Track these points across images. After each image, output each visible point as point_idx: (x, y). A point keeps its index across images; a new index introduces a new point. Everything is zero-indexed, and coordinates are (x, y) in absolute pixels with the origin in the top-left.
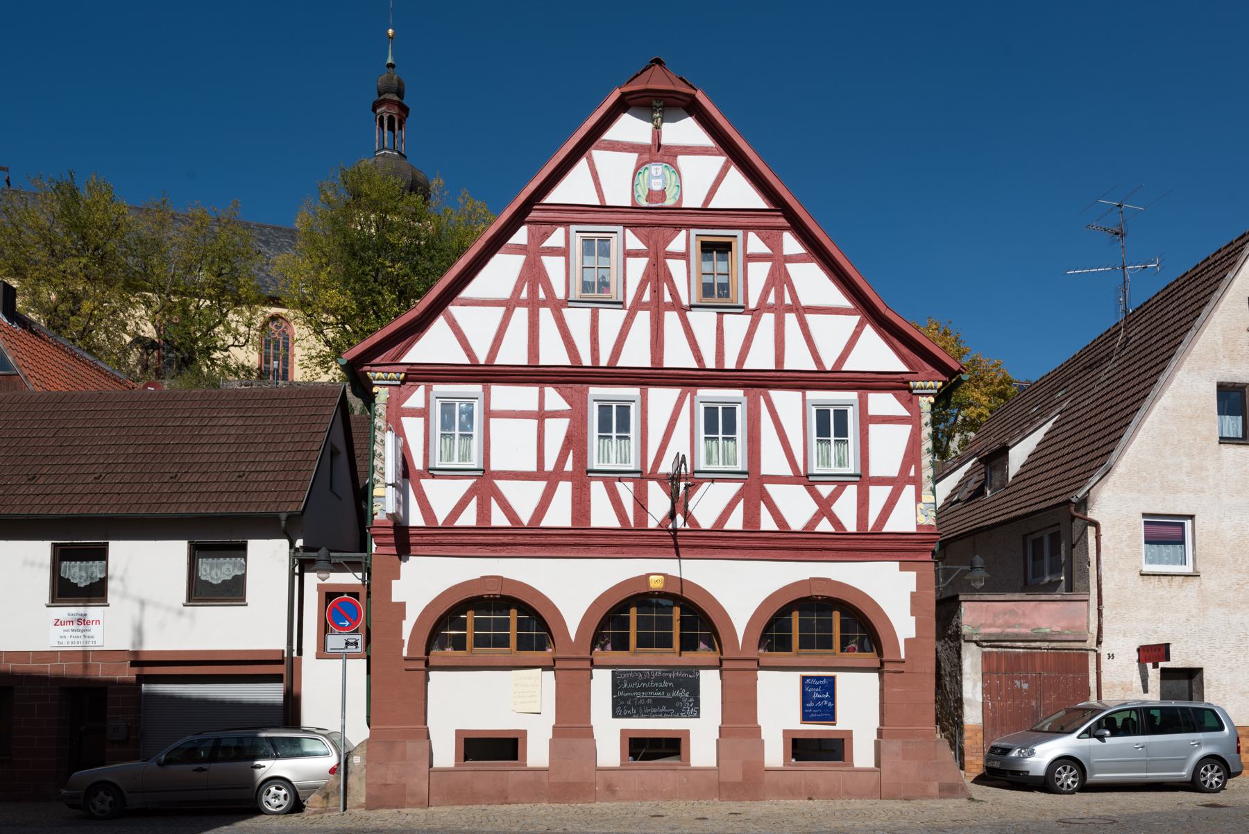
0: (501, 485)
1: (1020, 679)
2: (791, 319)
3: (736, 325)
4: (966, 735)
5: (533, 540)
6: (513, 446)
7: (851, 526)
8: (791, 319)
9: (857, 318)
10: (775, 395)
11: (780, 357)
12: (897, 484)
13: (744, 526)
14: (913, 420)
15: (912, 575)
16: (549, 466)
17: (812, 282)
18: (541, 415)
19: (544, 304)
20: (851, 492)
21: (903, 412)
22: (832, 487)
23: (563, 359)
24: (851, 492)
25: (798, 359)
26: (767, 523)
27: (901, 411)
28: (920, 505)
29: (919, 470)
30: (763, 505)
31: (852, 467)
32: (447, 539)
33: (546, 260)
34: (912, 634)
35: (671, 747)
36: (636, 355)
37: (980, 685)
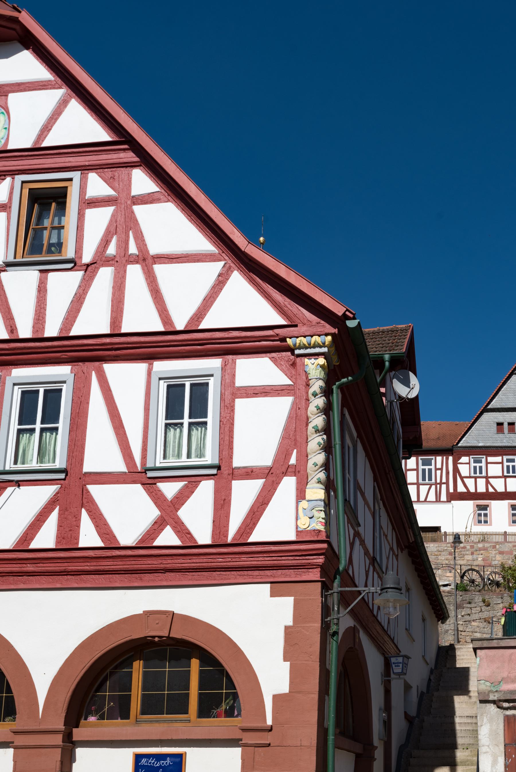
2: (134, 273)
3: (63, 285)
7: (203, 535)
8: (134, 273)
9: (218, 266)
10: (111, 369)
12: (270, 477)
13: (58, 542)
14: (298, 389)
15: (287, 604)
17: (166, 226)
20: (206, 489)
21: (284, 380)
22: (178, 485)
24: (206, 489)
25: (141, 318)
27: (279, 378)
28: (303, 504)
29: (304, 457)
30: (84, 515)
31: (210, 457)
34: (284, 688)
37: (501, 761)
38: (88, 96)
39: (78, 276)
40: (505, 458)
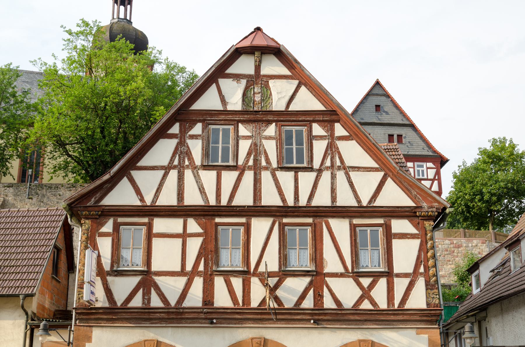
0: (157, 279)
2: (340, 175)
3: (306, 179)
6: (166, 256)
7: (383, 305)
8: (340, 175)
16: (189, 267)
18: (184, 236)
20: (383, 282)
21: (414, 231)
23: (277, 202)
24: (383, 282)
25: (346, 199)
26: (328, 303)
33: (190, 142)
39: (314, 175)
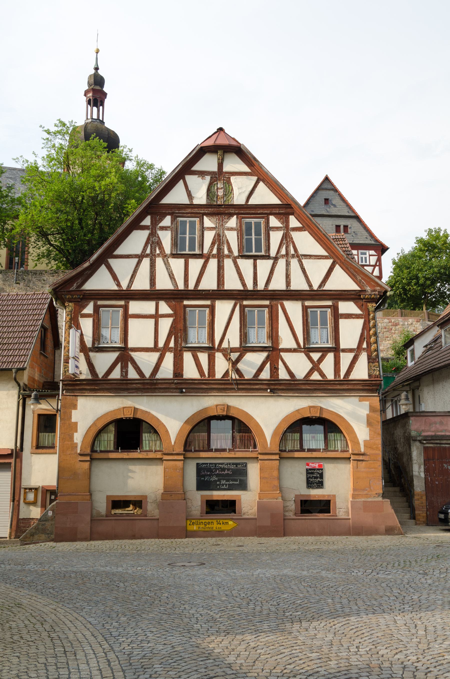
1: (446, 463)
2: (294, 262)
3: (264, 266)
4: (416, 497)
5: (150, 386)
6: (141, 334)
7: (330, 376)
8: (294, 262)
10: (288, 304)
11: (288, 283)
16: (161, 344)
18: (156, 317)
19: (293, 256)
20: (330, 357)
23: (169, 286)
24: (330, 357)
25: (299, 284)
26: (283, 375)
27: (357, 311)
32: (97, 385)
35: (230, 506)
36: (209, 283)
38: (341, 382)
39: (271, 262)
40: (360, 251)
